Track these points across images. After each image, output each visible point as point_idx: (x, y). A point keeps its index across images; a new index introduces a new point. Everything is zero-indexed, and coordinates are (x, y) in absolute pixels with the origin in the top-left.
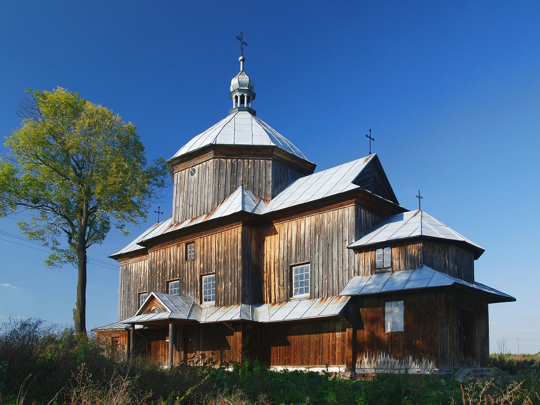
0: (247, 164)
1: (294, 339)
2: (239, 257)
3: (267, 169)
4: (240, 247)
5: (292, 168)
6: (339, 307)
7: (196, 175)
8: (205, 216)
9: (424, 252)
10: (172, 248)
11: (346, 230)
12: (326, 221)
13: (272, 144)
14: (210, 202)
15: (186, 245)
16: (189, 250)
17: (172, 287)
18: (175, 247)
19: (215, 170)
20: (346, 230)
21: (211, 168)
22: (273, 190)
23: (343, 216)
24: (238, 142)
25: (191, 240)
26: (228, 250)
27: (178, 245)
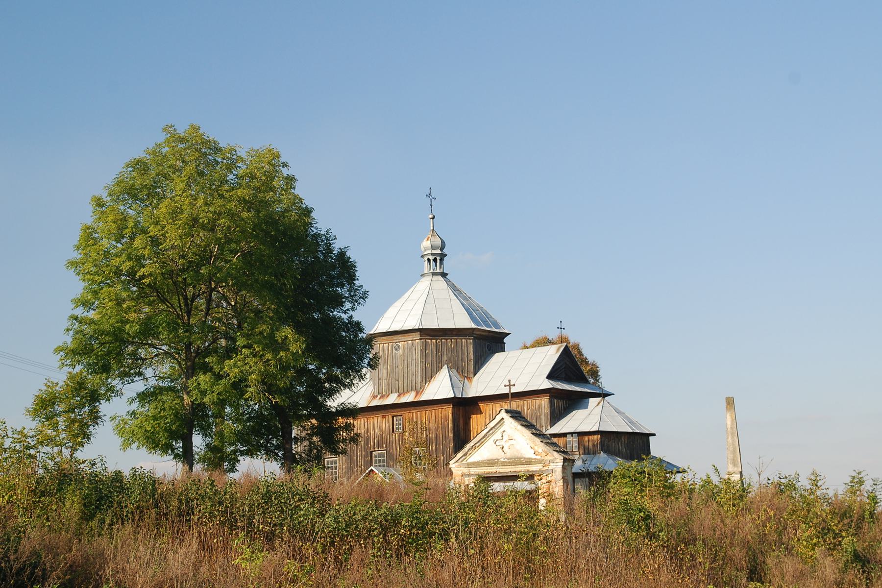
0: (450, 343)
1: (481, 405)
2: (451, 435)
3: (468, 346)
4: (451, 426)
5: (489, 342)
6: (558, 349)
7: (401, 351)
8: (413, 393)
9: (602, 443)
10: (376, 419)
11: (543, 418)
12: (525, 408)
13: (474, 326)
14: (419, 379)
15: (393, 417)
16: (395, 422)
17: (376, 457)
18: (380, 418)
19: (421, 350)
20: (543, 418)
21: (418, 348)
22: (475, 368)
23: (540, 406)
24: (441, 327)
25: (399, 414)
26: (438, 426)
27: (383, 417)
